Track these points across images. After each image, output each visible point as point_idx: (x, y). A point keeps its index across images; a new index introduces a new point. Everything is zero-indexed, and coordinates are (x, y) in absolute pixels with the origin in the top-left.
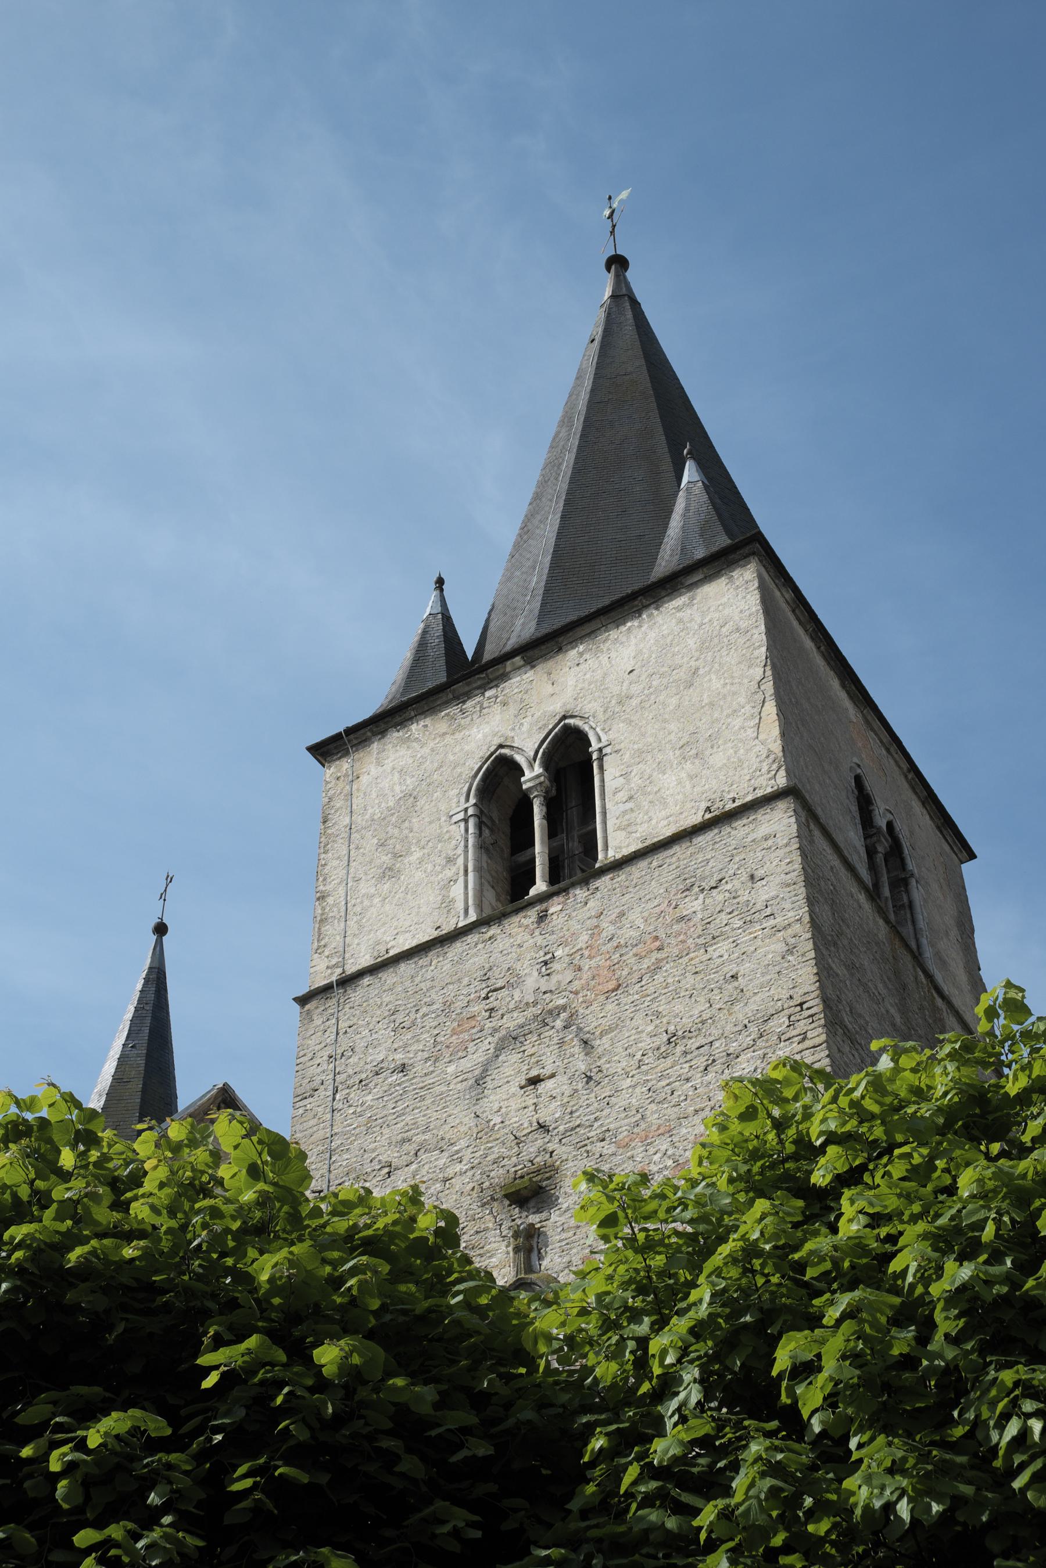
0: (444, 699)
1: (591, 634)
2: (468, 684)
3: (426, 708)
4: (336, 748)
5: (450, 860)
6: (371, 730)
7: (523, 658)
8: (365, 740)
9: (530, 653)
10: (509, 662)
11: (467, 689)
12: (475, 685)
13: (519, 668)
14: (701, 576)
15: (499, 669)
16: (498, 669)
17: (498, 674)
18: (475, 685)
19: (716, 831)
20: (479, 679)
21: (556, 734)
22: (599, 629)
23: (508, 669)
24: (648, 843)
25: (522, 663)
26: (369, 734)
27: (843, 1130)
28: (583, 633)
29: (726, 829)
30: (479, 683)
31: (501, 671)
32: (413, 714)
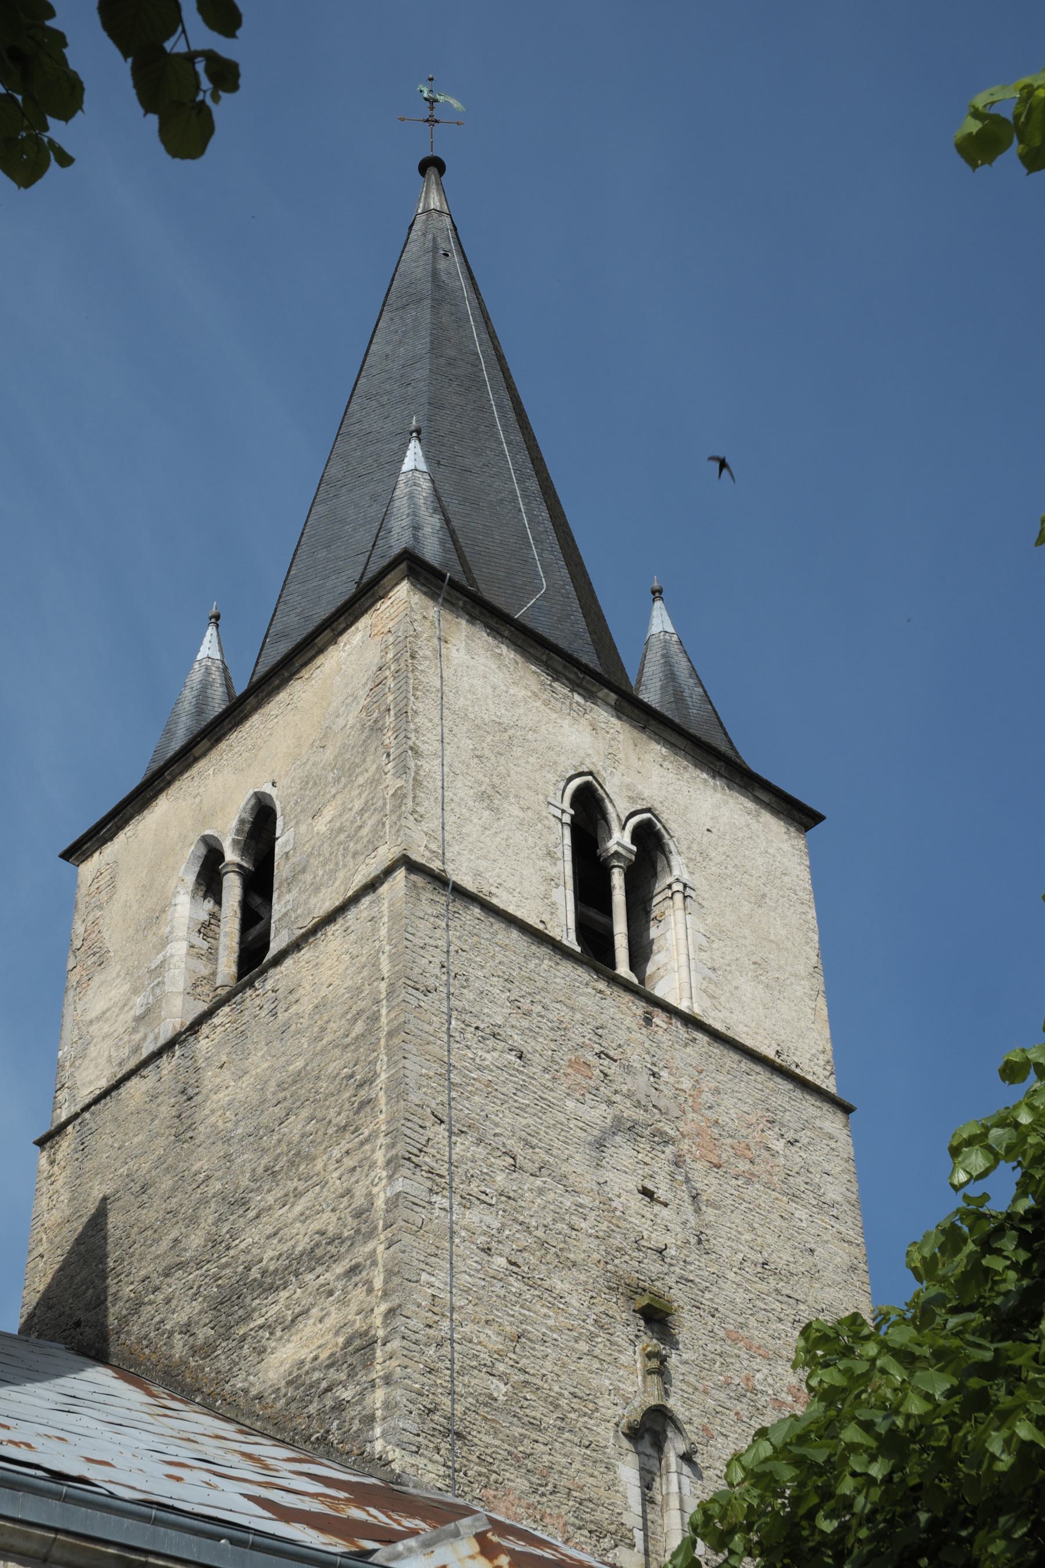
0: (538, 654)
1: (557, 676)
2: (565, 667)
3: (519, 643)
4: (426, 579)
5: (614, 878)
6: (465, 603)
7: (617, 700)
8: (453, 604)
9: (625, 704)
10: (606, 690)
11: (560, 669)
12: (531, 651)
13: (607, 704)
14: (767, 800)
15: (595, 686)
16: (594, 685)
17: (590, 688)
18: (567, 674)
19: (791, 1087)
20: (576, 673)
21: (596, 790)
22: (680, 749)
23: (600, 694)
24: (729, 1033)
25: (613, 703)
26: (461, 603)
27: (423, 1525)
28: (668, 737)
29: (798, 1094)
30: (572, 676)
31: (594, 689)
32: (506, 633)
